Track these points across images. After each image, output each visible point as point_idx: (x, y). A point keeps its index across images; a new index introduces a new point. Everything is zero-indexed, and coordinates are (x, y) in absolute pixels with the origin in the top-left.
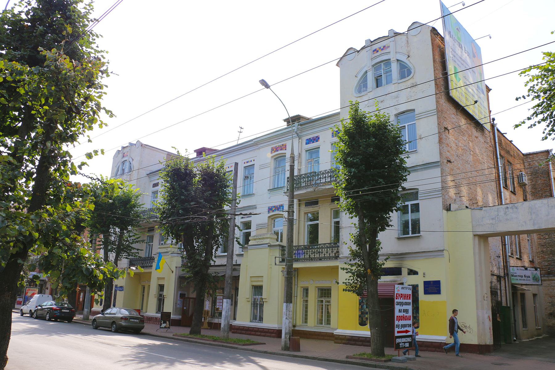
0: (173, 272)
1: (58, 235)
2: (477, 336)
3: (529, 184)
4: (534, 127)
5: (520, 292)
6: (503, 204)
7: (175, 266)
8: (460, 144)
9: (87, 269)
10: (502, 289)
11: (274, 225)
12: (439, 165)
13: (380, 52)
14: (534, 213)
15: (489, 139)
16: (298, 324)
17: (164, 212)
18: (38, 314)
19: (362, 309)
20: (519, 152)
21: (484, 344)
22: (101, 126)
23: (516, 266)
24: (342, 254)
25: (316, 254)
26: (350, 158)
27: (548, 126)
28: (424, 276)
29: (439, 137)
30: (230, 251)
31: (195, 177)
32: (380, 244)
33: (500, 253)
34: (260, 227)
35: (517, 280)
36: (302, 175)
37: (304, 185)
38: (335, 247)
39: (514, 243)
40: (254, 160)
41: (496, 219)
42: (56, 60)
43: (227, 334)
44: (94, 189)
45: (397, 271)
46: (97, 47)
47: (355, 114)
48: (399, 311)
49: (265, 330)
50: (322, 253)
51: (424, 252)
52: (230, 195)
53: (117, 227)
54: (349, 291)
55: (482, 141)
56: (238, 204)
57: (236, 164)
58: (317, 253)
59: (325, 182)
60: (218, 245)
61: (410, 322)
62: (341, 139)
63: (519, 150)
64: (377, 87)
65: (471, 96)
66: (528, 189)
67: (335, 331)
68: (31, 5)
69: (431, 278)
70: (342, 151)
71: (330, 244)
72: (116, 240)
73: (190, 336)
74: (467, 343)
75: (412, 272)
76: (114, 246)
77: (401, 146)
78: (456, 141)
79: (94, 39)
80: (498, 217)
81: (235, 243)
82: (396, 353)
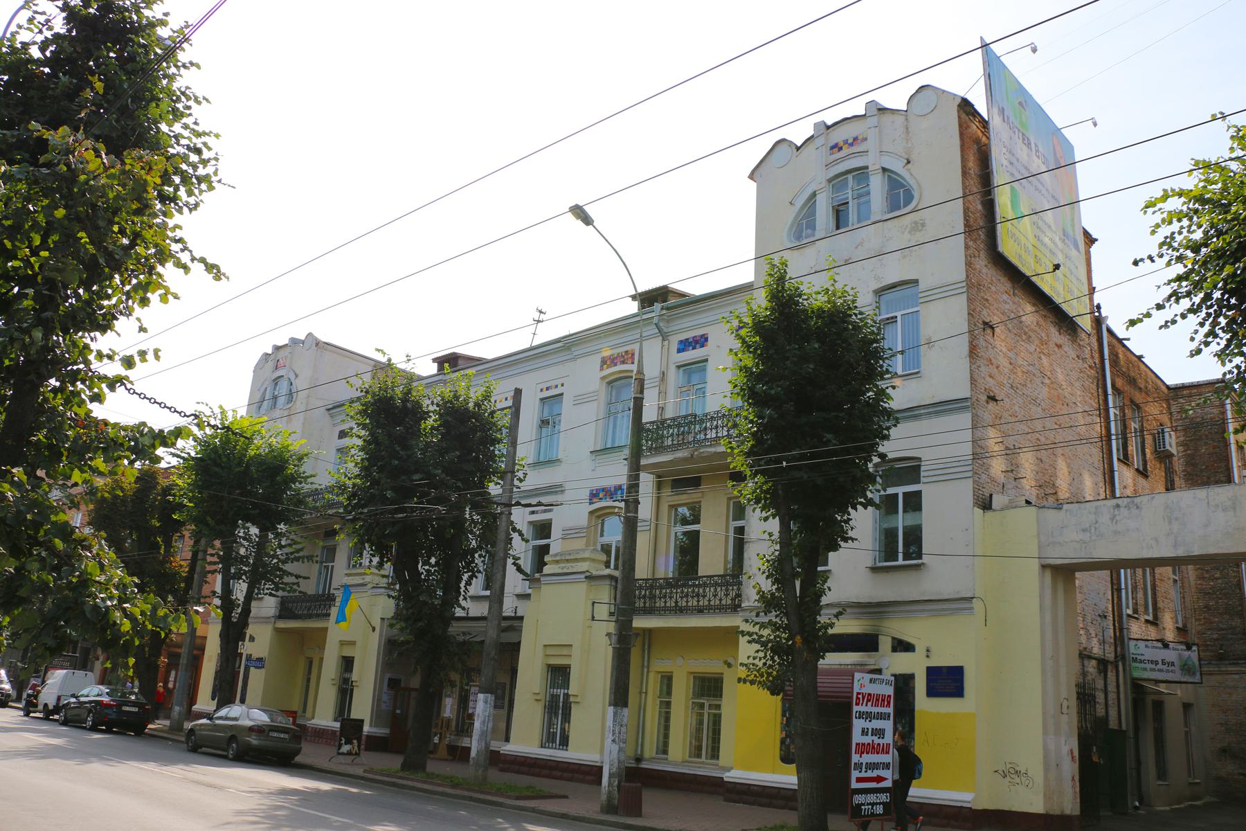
0: (374, 629)
2: (1042, 795)
3: (1180, 455)
4: (1172, 327)
6: (1118, 495)
7: (380, 616)
8: (1020, 362)
10: (1109, 689)
11: (602, 531)
12: (967, 407)
14: (1176, 519)
15: (1087, 350)
16: (647, 755)
17: (354, 495)
18: (68, 715)
20: (1159, 382)
21: (1059, 813)
22: (164, 299)
25: (690, 599)
26: (763, 386)
27: (1202, 325)
28: (928, 656)
29: (971, 343)
30: (497, 586)
31: (426, 419)
33: (1107, 608)
34: (567, 535)
35: (1145, 669)
36: (666, 420)
39: (1140, 586)
40: (562, 385)
42: (69, 151)
43: (483, 771)
44: (134, 435)
45: (866, 643)
46: (196, 123)
47: (778, 285)
48: (863, 731)
50: (704, 596)
51: (931, 601)
52: (502, 461)
53: (253, 524)
54: (752, 683)
55: (1072, 354)
56: (521, 481)
57: (518, 392)
58: (693, 597)
59: (717, 437)
60: (472, 571)
62: (744, 342)
64: (838, 228)
66: (1178, 465)
67: (727, 774)
68: (51, 30)
69: (942, 660)
70: (745, 369)
72: (250, 554)
73: (400, 774)
74: (1006, 809)
75: (902, 646)
76: (244, 568)
77: (881, 362)
78: (1011, 354)
79: (189, 108)
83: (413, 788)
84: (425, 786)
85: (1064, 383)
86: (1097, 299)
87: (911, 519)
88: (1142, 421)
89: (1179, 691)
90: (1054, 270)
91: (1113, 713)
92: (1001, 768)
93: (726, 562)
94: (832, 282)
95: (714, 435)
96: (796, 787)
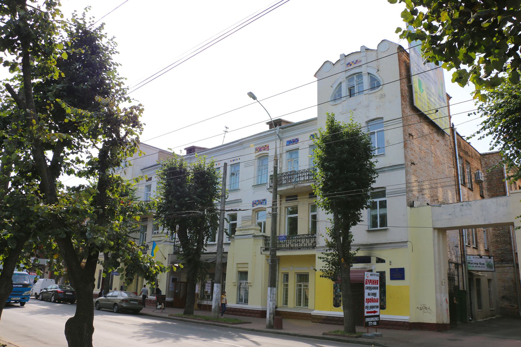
0: (165, 259)
1: (120, 241)
2: (435, 316)
4: (483, 139)
5: (476, 277)
6: (462, 201)
7: (168, 253)
8: (423, 148)
9: (145, 266)
10: (459, 275)
12: (404, 167)
13: (354, 66)
14: (485, 210)
15: (449, 142)
16: (279, 305)
18: (43, 297)
19: (336, 293)
20: (477, 152)
23: (473, 254)
24: (319, 244)
25: (295, 244)
27: (494, 139)
28: (390, 264)
31: (188, 175)
32: (352, 236)
33: (458, 243)
34: (244, 218)
35: (473, 267)
36: (283, 173)
37: (285, 182)
38: (313, 238)
39: (471, 234)
40: (239, 159)
41: (453, 215)
45: (366, 260)
47: (331, 124)
48: (368, 294)
49: (250, 311)
50: (301, 243)
54: (325, 277)
55: (443, 144)
58: (296, 243)
59: (304, 180)
61: (378, 304)
63: (477, 151)
65: (433, 105)
67: (313, 312)
70: (320, 157)
71: (308, 235)
75: (380, 261)
77: (371, 152)
78: (419, 146)
80: (455, 213)
81: (225, 234)
82: (365, 330)
83: (191, 321)
84: (195, 320)
85: (440, 156)
86: (452, 121)
87: (383, 211)
88: (470, 169)
89: (486, 274)
90: (436, 112)
91: (461, 284)
92: (419, 307)
93: (309, 229)
94: (351, 121)
95: (303, 179)
96: (343, 316)
